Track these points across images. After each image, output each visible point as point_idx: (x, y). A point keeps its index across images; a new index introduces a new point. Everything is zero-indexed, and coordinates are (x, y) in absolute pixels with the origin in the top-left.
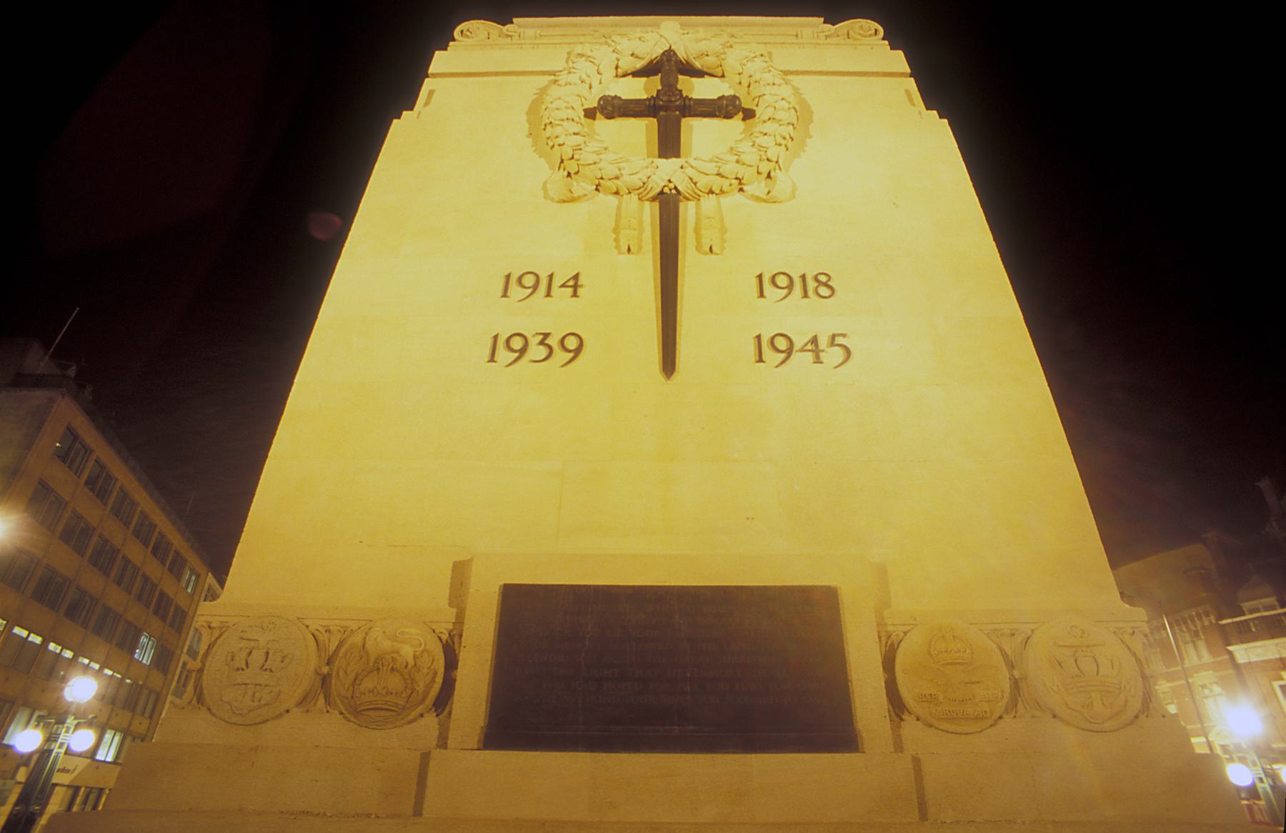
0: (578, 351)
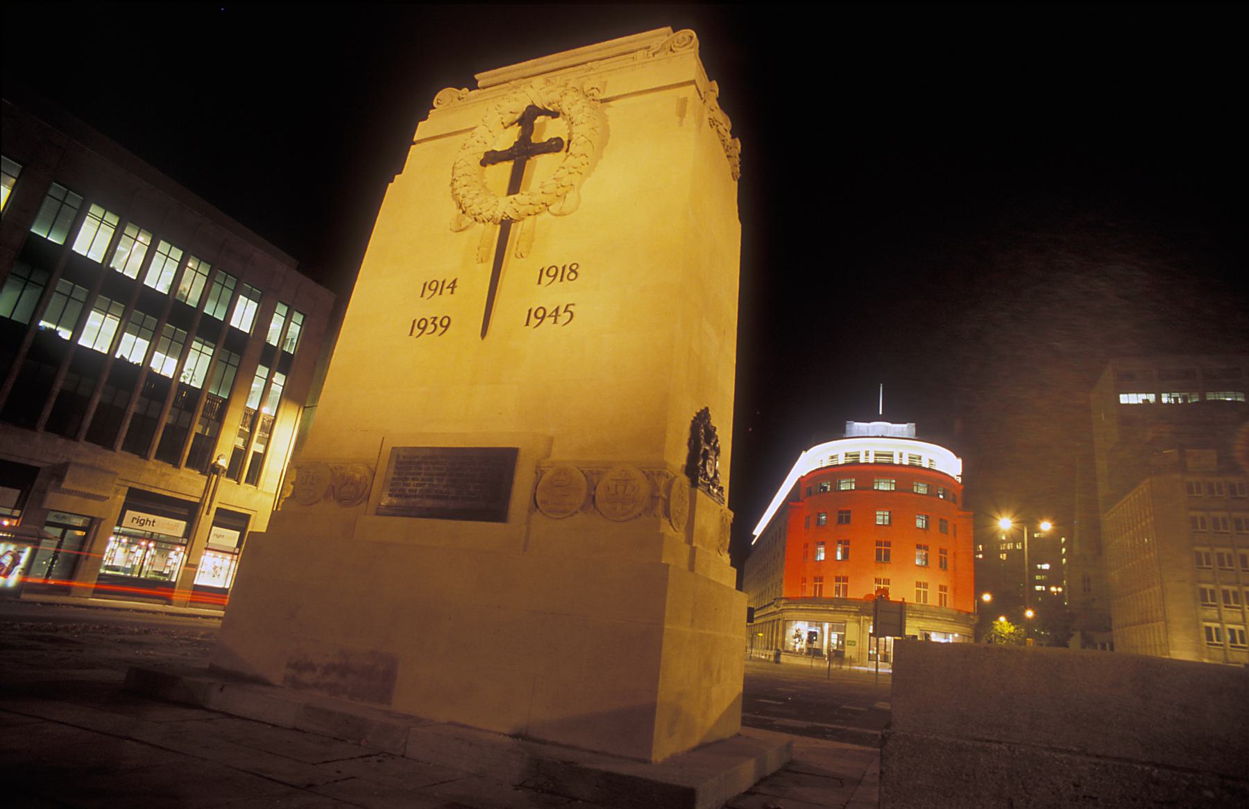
0: (447, 327)
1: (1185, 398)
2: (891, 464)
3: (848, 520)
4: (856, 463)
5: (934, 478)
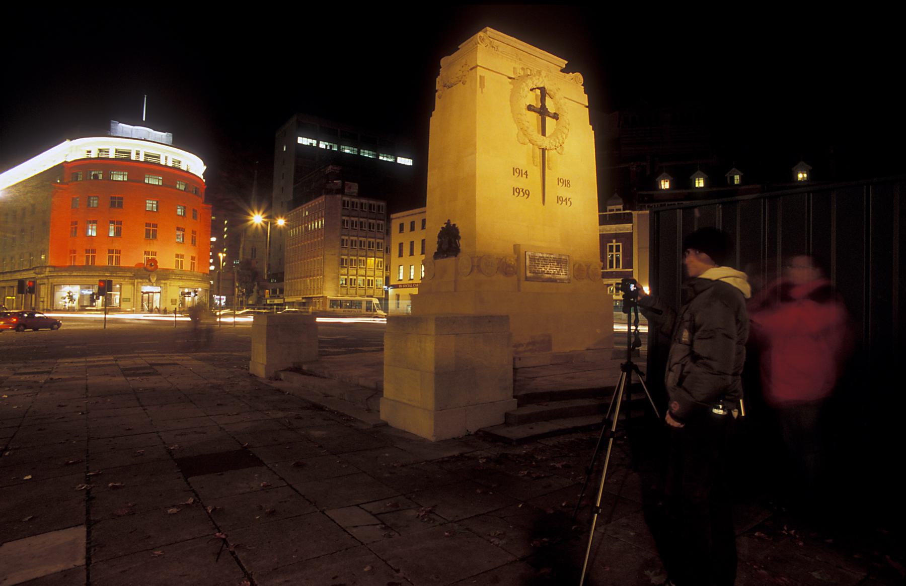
1: (331, 147)
2: (159, 164)
3: (120, 205)
4: (128, 159)
5: (187, 176)
